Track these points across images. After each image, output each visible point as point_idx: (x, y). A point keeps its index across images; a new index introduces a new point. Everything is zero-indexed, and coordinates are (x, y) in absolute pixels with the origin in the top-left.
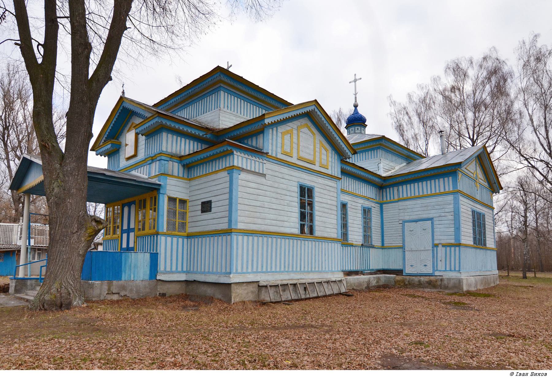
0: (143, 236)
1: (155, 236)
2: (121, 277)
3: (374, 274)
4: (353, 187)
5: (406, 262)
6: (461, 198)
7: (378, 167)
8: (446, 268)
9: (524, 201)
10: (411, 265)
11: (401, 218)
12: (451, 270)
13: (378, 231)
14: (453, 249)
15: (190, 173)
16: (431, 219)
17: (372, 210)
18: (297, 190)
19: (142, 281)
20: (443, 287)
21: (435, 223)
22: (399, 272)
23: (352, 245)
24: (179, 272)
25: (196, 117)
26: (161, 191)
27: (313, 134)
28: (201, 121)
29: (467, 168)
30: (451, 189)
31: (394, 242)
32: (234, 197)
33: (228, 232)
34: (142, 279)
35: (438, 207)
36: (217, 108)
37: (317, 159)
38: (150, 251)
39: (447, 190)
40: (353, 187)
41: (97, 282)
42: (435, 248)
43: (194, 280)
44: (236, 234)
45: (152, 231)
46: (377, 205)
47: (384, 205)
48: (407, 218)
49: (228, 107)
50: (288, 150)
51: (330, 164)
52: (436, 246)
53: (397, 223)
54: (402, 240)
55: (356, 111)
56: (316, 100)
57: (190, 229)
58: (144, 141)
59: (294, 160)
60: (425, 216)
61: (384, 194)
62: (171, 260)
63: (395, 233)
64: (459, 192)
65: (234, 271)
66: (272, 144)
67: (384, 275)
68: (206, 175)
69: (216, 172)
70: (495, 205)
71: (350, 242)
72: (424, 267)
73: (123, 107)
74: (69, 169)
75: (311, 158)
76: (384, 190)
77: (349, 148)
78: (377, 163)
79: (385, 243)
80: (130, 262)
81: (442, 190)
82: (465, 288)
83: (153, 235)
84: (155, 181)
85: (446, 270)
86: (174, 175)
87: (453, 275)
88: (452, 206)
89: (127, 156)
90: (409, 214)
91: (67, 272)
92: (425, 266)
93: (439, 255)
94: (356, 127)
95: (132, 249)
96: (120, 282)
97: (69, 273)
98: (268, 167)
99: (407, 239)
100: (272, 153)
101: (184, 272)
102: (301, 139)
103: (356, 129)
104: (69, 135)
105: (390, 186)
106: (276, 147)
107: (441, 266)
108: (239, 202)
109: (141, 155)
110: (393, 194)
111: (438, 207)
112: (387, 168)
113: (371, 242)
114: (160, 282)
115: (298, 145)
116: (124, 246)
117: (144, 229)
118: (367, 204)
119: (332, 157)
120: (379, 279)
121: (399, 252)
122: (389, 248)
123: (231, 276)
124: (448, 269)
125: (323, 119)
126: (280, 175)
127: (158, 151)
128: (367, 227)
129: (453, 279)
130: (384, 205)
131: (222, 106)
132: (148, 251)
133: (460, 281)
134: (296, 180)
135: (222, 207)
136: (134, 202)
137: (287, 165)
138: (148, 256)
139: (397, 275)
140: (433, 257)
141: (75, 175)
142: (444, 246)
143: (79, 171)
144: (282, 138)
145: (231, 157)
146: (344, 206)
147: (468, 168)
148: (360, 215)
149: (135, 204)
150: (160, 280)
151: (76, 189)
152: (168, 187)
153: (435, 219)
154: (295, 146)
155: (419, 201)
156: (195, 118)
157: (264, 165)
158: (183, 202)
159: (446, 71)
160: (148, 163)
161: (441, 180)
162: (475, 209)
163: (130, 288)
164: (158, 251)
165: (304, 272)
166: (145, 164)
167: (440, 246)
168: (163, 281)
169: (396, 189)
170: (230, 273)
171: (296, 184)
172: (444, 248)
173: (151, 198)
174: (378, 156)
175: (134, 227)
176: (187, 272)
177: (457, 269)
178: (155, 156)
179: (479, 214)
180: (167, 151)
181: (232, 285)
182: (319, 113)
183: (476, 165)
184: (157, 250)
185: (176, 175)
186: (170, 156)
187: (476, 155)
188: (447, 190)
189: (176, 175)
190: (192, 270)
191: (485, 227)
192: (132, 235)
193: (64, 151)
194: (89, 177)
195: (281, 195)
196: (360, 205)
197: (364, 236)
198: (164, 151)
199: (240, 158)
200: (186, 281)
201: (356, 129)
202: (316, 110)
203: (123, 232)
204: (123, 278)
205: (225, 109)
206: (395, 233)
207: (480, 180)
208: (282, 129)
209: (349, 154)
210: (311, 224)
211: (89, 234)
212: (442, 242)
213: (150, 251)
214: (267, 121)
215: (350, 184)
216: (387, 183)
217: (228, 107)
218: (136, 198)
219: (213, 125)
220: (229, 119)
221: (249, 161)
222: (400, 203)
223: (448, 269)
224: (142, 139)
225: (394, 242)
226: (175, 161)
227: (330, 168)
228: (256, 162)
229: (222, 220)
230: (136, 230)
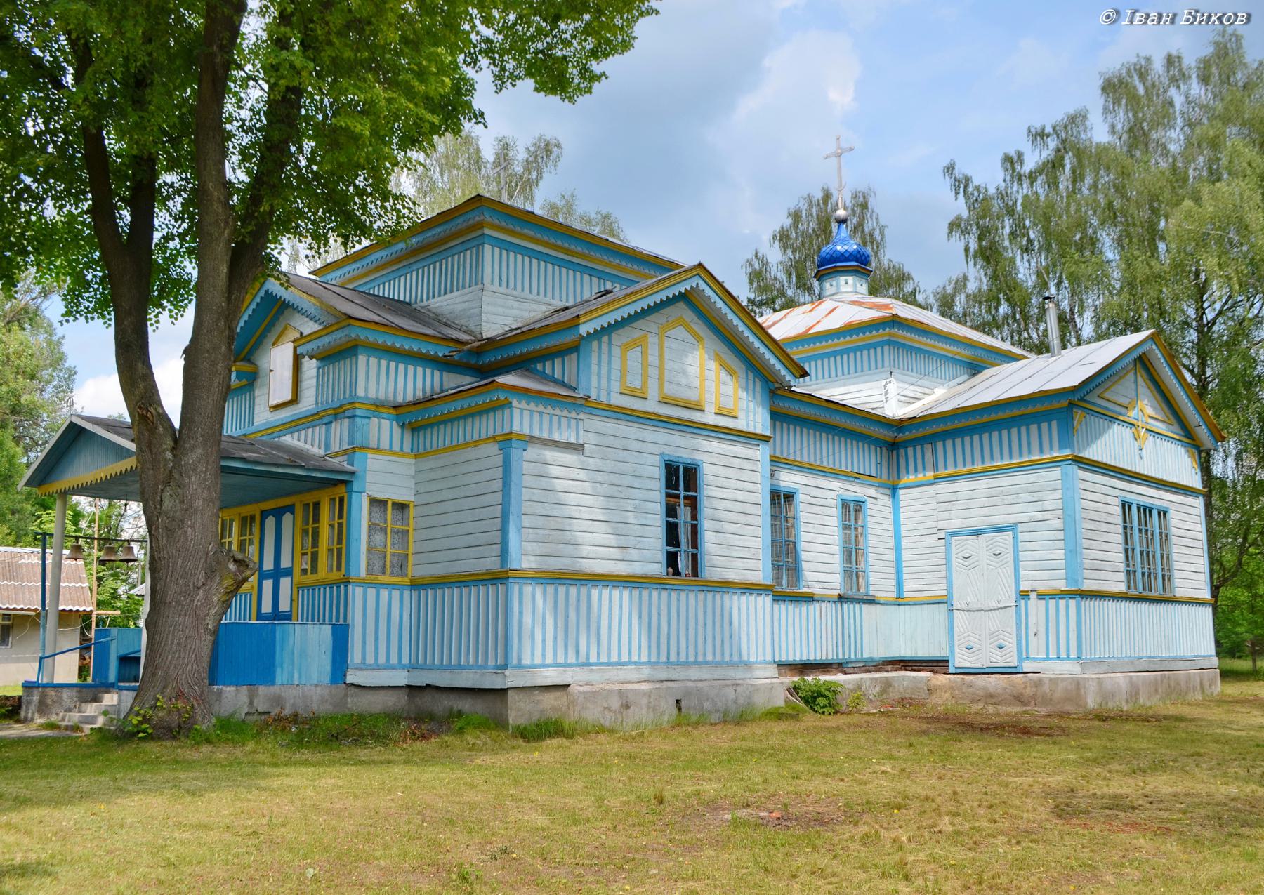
0: (312, 587)
1: (342, 587)
2: (275, 677)
7: (886, 393)
8: (1047, 654)
10: (966, 645)
11: (942, 525)
16: (1011, 528)
17: (869, 506)
18: (659, 473)
19: (316, 686)
20: (1039, 699)
21: (1021, 536)
23: (809, 598)
24: (393, 668)
25: (428, 299)
28: (439, 311)
32: (513, 501)
34: (315, 682)
38: (331, 620)
41: (228, 689)
42: (1023, 602)
43: (428, 685)
44: (517, 580)
45: (336, 575)
46: (881, 490)
48: (956, 525)
49: (500, 279)
50: (637, 384)
56: (700, 265)
57: (413, 570)
58: (315, 370)
59: (651, 406)
60: (997, 520)
62: (377, 639)
65: (515, 662)
66: (599, 375)
67: (903, 673)
68: (453, 448)
69: (475, 443)
72: (998, 652)
73: (267, 291)
74: (191, 461)
76: (902, 451)
77: (787, 364)
78: (884, 382)
80: (291, 642)
82: (1092, 702)
83: (337, 584)
84: (340, 462)
85: (1047, 659)
86: (381, 447)
88: (1058, 495)
89: (274, 402)
91: (187, 666)
93: (1032, 620)
95: (288, 616)
96: (272, 689)
97: (189, 668)
98: (591, 429)
99: (957, 581)
100: (598, 395)
101: (403, 667)
102: (667, 354)
105: (914, 442)
106: (609, 379)
107: (1036, 647)
108: (524, 510)
109: (308, 402)
112: (912, 395)
113: (867, 587)
114: (353, 690)
115: (661, 369)
116: (267, 608)
117: (314, 568)
120: (887, 684)
123: (508, 672)
124: (1052, 655)
125: (720, 304)
126: (618, 443)
127: (347, 396)
128: (852, 552)
131: (487, 280)
132: (324, 620)
133: (1078, 684)
135: (487, 522)
136: (291, 509)
137: (635, 419)
138: (327, 630)
139: (935, 672)
141: (202, 471)
142: (1041, 596)
143: (207, 463)
144: (623, 359)
145: (507, 412)
146: (781, 500)
147: (1106, 395)
148: (833, 518)
149: (293, 513)
150: (352, 684)
151: (203, 500)
152: (370, 478)
154: (653, 372)
156: (425, 303)
157: (581, 423)
158: (401, 507)
159: (951, 231)
160: (325, 420)
162: (1131, 498)
163: (292, 701)
164: (350, 621)
165: (678, 664)
166: (318, 422)
167: (1033, 595)
168: (359, 686)
169: (928, 448)
170: (505, 667)
171: (657, 460)
173: (334, 500)
174: (887, 363)
175: (290, 565)
176: (412, 667)
178: (341, 407)
179: (1146, 511)
180: (366, 397)
181: (510, 693)
182: (708, 292)
183: (1136, 382)
184: (345, 619)
185: (387, 447)
186: (373, 408)
187: (1136, 354)
189: (387, 447)
190: (420, 661)
192: (285, 583)
193: (177, 425)
195: (620, 488)
198: (358, 398)
199: (526, 414)
200: (410, 688)
202: (702, 286)
203: (263, 576)
204: (278, 680)
205: (495, 287)
208: (619, 338)
209: (788, 377)
210: (694, 551)
211: (226, 588)
213: (331, 620)
214: (584, 329)
215: (831, 451)
217: (500, 279)
218: (296, 500)
219: (466, 324)
220: (503, 307)
221: (546, 418)
223: (1052, 655)
224: (310, 366)
226: (385, 416)
227: (741, 415)
229: (486, 551)
230: (297, 572)
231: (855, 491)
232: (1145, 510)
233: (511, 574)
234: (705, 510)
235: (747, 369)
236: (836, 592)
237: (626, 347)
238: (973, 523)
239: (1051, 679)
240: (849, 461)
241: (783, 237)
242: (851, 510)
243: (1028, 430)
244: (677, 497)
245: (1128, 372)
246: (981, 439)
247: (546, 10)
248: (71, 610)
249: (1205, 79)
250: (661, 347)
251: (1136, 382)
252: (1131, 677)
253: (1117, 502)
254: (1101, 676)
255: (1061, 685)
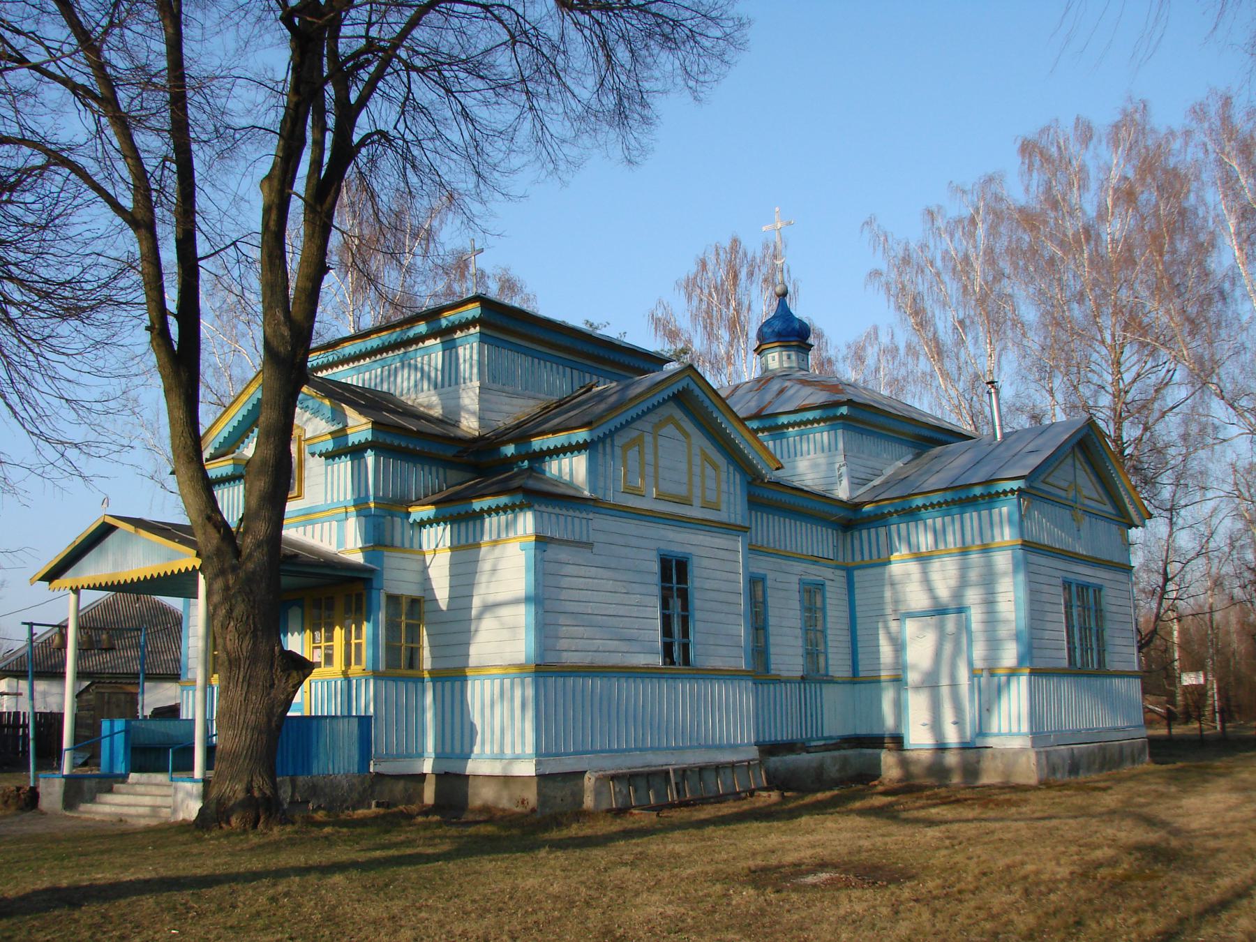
3: (834, 750)
4: (777, 533)
9: (556, 821)
13: (841, 638)
23: (778, 680)
26: (375, 585)
27: (686, 434)
29: (1047, 480)
37: (697, 492)
40: (777, 533)
47: (856, 573)
51: (724, 497)
70: (1136, 560)
71: (773, 672)
75: (682, 491)
79: (860, 668)
104: (830, 789)
110: (878, 545)
118: (817, 573)
119: (728, 482)
122: (870, 682)
130: (856, 573)
162: (1071, 576)
179: (1083, 587)
183: (1074, 466)
187: (1075, 441)
196: (795, 579)
197: (808, 653)
207: (1087, 502)
215: (771, 524)
227: (724, 507)
228: (576, 519)
231: (817, 573)
232: (1082, 589)
234: (696, 600)
235: (728, 463)
236: (801, 674)
237: (625, 448)
240: (765, 524)
241: (690, 286)
242: (812, 592)
244: (671, 588)
245: (1066, 457)
247: (1207, 648)
249: (1115, 142)
250: (656, 447)
251: (1074, 466)
252: (1072, 749)
253: (1059, 581)
254: (1048, 749)
255: (231, 639)
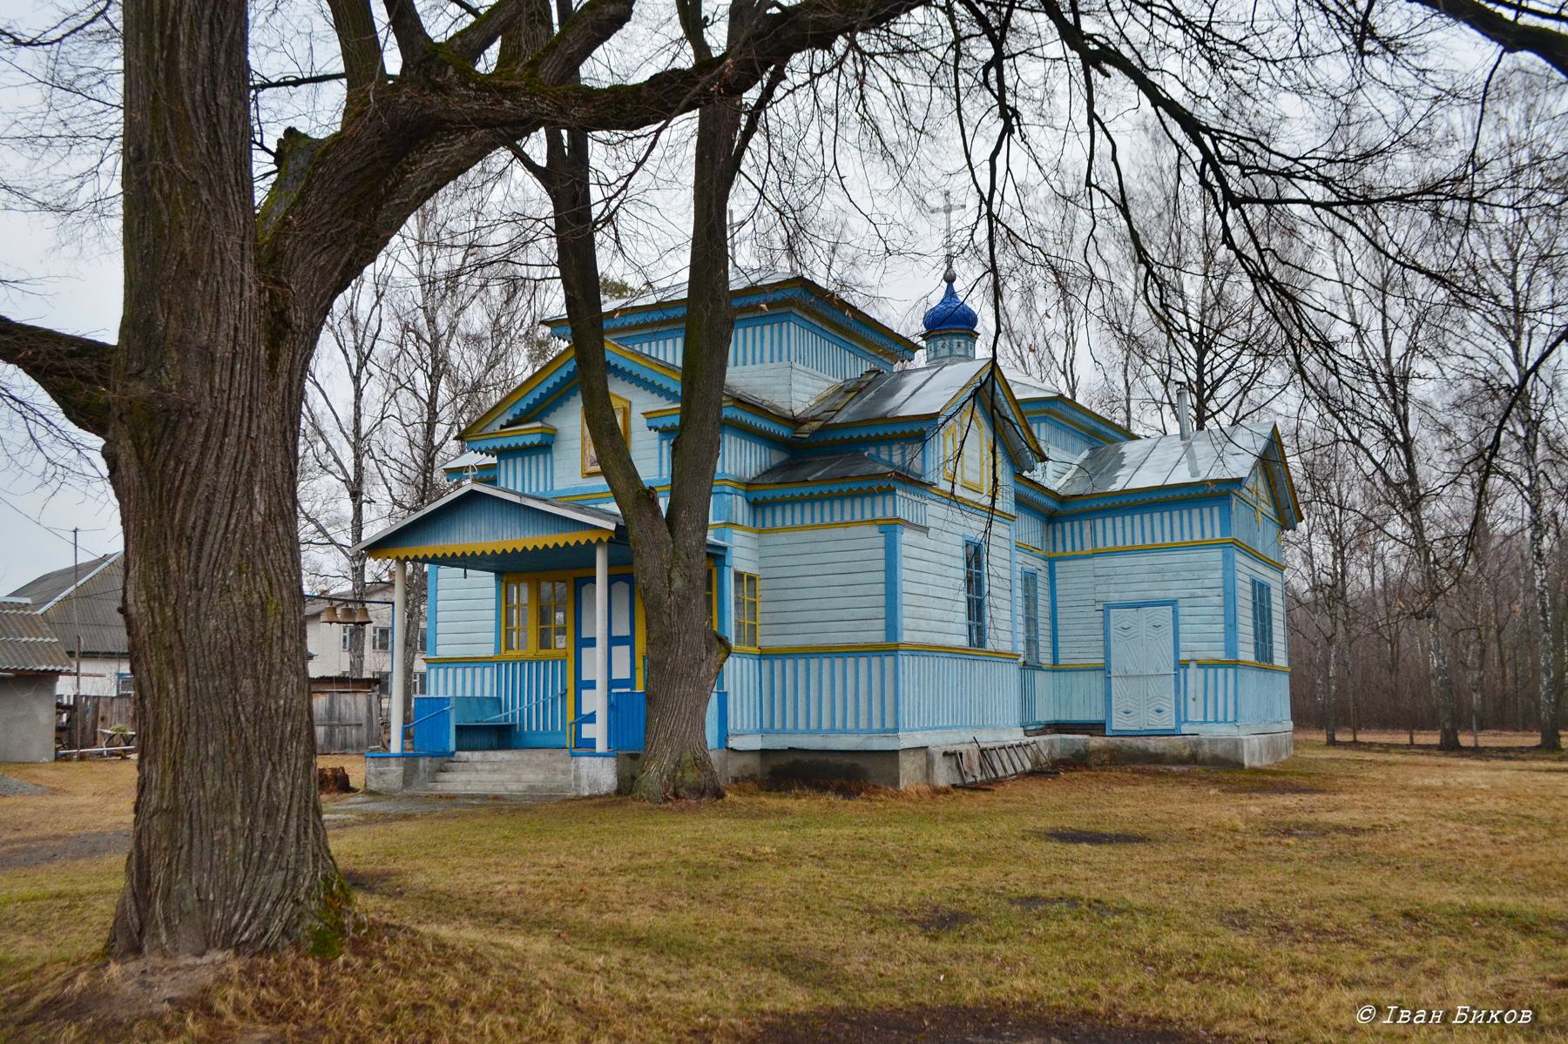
5: (1113, 702)
6: (1239, 557)
11: (1099, 597)
12: (1216, 721)
14: (1221, 672)
15: (759, 517)
16: (1173, 603)
21: (1181, 611)
22: (1096, 728)
30: (1218, 536)
31: (1081, 656)
33: (889, 648)
35: (1189, 575)
36: (780, 359)
39: (1208, 536)
42: (1182, 671)
47: (1057, 564)
48: (1115, 597)
52: (1182, 665)
53: (1092, 608)
54: (1102, 650)
55: (950, 293)
57: (765, 641)
60: (1158, 595)
61: (1059, 535)
63: (1086, 632)
64: (1235, 542)
72: (1156, 715)
76: (1059, 526)
81: (1197, 537)
85: (1205, 722)
87: (1223, 731)
88: (1219, 574)
90: (1119, 587)
92: (1159, 711)
93: (1191, 686)
94: (955, 341)
99: (1116, 650)
103: (955, 346)
107: (1194, 711)
108: (905, 589)
111: (1189, 575)
121: (1097, 680)
122: (1071, 671)
129: (1222, 740)
130: (1057, 564)
133: (1236, 744)
134: (960, 530)
140: (1177, 691)
142: (1200, 665)
153: (1181, 603)
155: (1144, 560)
158: (752, 579)
161: (1196, 512)
167: (1192, 665)
171: (960, 541)
172: (1202, 671)
176: (763, 732)
177: (889, 724)
179: (1262, 585)
188: (1208, 536)
191: (1270, 615)
194: (708, 555)
201: (955, 346)
206: (1086, 632)
212: (1197, 656)
216: (1069, 509)
222: (1098, 561)
225: (1081, 656)
233: (901, 647)
238: (1132, 596)
239: (1210, 741)
243: (1190, 514)
246: (1142, 519)
248: (45, 671)
